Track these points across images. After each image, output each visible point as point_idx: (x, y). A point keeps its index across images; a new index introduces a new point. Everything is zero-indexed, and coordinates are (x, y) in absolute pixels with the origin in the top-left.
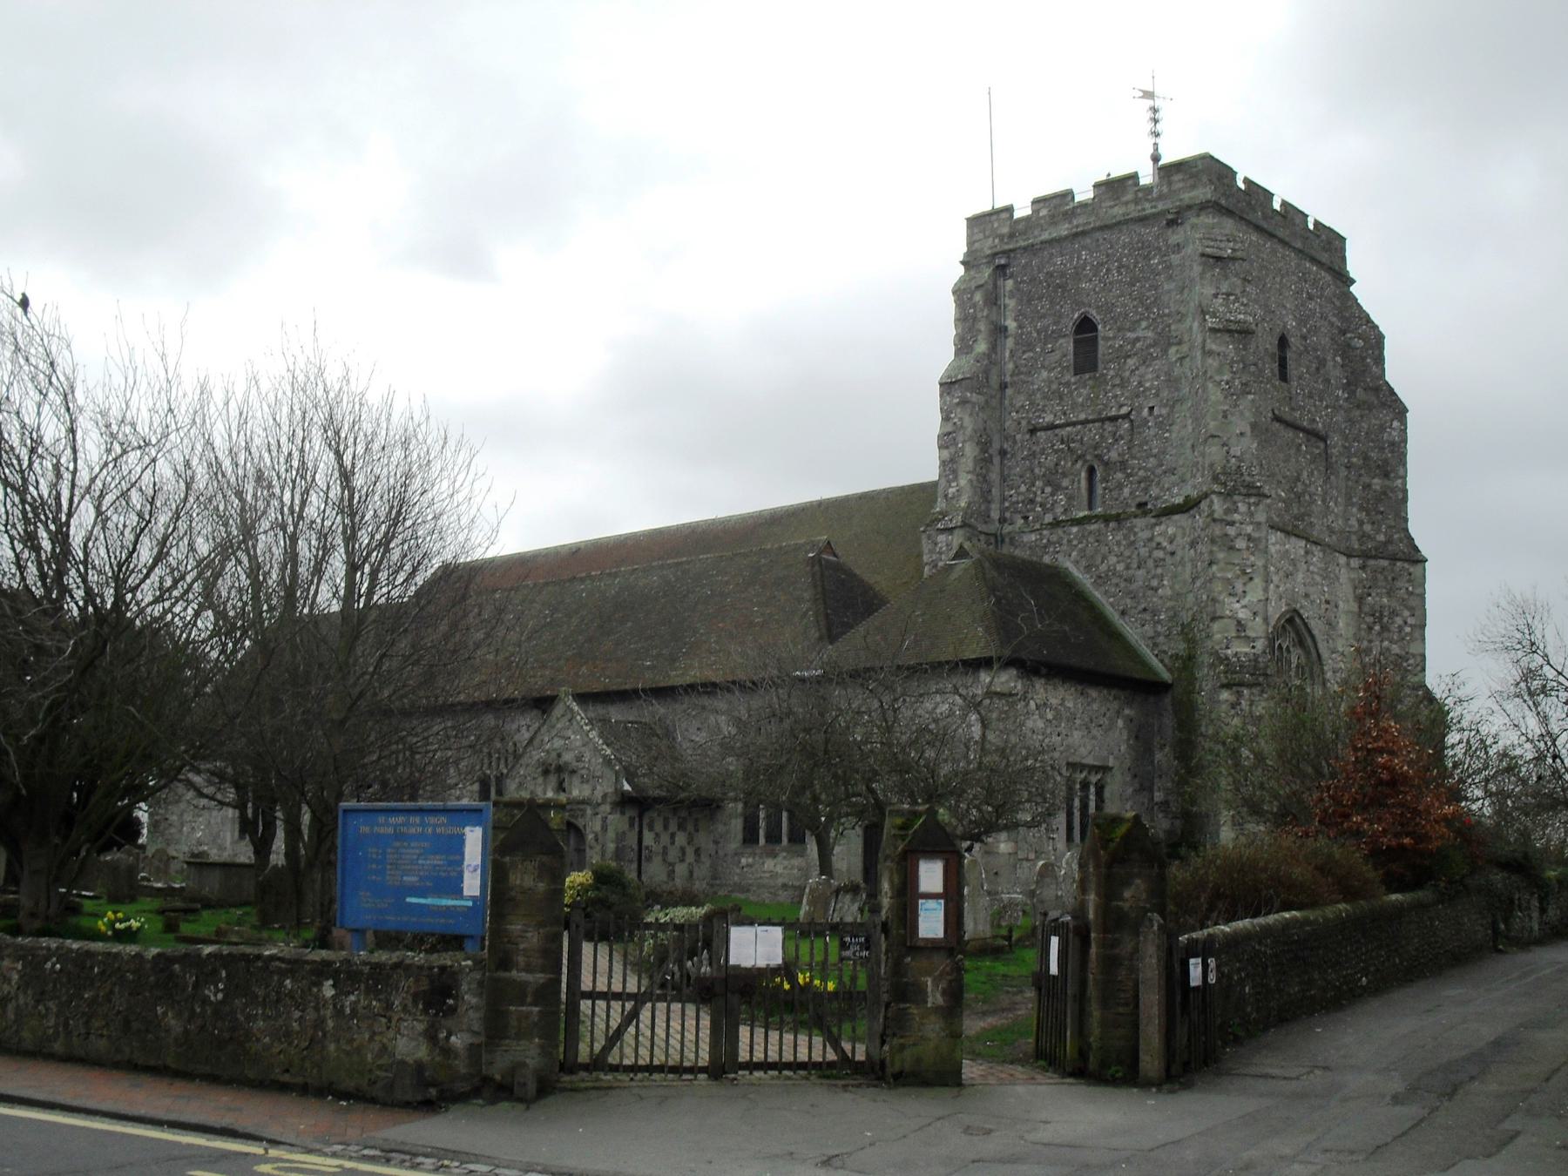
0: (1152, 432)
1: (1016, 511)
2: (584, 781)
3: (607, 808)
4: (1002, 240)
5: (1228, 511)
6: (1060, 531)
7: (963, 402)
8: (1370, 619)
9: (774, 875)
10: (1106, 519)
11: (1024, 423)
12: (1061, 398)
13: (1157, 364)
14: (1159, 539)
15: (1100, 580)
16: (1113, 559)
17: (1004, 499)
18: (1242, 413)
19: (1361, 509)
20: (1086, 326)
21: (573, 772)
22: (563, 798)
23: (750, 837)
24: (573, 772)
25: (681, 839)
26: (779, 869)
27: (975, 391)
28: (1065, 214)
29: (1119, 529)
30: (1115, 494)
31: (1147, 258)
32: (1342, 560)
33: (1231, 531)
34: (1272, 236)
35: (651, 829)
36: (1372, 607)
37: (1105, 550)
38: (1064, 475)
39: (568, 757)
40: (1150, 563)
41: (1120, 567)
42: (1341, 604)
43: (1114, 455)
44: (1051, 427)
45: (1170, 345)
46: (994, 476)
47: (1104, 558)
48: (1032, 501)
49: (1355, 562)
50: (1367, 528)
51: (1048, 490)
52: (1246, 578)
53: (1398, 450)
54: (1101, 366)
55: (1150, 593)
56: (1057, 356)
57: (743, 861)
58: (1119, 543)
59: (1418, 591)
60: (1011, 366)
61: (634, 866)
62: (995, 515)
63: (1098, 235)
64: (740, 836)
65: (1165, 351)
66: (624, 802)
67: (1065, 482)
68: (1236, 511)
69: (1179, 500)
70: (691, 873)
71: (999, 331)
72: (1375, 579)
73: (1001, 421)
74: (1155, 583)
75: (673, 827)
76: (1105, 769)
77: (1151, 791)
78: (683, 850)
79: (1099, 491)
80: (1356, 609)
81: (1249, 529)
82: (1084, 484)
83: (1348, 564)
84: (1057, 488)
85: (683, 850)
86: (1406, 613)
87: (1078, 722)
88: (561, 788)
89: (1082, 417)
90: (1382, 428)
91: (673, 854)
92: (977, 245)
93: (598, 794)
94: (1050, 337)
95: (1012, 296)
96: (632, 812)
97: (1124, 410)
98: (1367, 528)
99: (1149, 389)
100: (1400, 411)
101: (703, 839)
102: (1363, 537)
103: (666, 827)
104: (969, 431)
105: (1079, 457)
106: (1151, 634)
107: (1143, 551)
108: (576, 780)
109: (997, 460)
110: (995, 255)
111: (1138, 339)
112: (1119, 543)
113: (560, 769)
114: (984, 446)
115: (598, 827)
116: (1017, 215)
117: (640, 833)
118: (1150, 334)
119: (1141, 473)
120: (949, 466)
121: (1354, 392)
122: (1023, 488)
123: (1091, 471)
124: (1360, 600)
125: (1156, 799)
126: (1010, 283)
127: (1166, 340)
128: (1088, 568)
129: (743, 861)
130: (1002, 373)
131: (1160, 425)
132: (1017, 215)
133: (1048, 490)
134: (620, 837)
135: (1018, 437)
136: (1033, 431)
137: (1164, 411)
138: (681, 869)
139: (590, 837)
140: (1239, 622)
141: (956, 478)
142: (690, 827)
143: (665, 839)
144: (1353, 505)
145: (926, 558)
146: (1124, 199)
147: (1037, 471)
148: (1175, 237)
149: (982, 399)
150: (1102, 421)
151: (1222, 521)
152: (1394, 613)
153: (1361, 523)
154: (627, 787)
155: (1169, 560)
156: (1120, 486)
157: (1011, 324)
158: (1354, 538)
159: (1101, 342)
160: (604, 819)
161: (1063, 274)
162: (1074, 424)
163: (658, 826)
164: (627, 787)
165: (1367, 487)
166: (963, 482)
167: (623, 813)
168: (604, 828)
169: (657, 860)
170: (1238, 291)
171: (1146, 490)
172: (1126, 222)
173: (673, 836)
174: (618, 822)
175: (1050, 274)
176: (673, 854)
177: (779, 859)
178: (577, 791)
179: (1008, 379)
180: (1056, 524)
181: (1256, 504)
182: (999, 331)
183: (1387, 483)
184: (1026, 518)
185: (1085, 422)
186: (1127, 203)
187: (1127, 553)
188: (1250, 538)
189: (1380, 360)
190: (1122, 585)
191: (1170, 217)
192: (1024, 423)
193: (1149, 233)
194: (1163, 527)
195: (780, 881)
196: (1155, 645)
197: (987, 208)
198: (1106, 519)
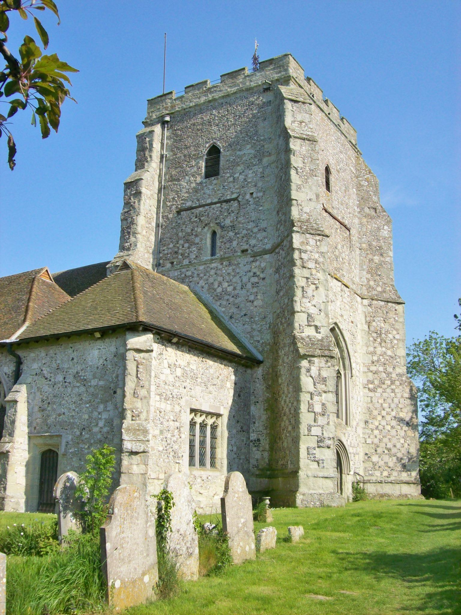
5: (302, 243)
6: (192, 269)
8: (375, 335)
11: (174, 207)
13: (255, 168)
16: (225, 285)
18: (310, 188)
19: (368, 272)
20: (214, 151)
29: (230, 264)
32: (359, 299)
34: (323, 111)
37: (220, 279)
38: (196, 236)
41: (230, 289)
42: (359, 326)
43: (228, 222)
48: (176, 253)
49: (366, 302)
50: (372, 283)
51: (186, 245)
54: (221, 172)
65: (260, 160)
67: (197, 240)
74: (252, 298)
76: (218, 415)
77: (248, 433)
79: (218, 244)
80: (367, 329)
81: (316, 256)
83: (362, 303)
84: (192, 244)
86: (395, 332)
87: (199, 380)
89: (209, 201)
90: (379, 229)
97: (234, 196)
98: (372, 283)
102: (370, 288)
105: (206, 225)
106: (249, 329)
107: (245, 279)
119: (245, 232)
121: (363, 209)
122: (171, 246)
123: (214, 233)
124: (369, 324)
125: (251, 438)
133: (186, 245)
144: (364, 270)
147: (180, 234)
152: (387, 332)
153: (369, 280)
155: (262, 283)
156: (231, 241)
158: (364, 288)
162: (203, 206)
165: (371, 260)
170: (306, 121)
183: (382, 259)
187: (234, 280)
188: (316, 262)
190: (232, 299)
194: (258, 263)
197: (162, 94)
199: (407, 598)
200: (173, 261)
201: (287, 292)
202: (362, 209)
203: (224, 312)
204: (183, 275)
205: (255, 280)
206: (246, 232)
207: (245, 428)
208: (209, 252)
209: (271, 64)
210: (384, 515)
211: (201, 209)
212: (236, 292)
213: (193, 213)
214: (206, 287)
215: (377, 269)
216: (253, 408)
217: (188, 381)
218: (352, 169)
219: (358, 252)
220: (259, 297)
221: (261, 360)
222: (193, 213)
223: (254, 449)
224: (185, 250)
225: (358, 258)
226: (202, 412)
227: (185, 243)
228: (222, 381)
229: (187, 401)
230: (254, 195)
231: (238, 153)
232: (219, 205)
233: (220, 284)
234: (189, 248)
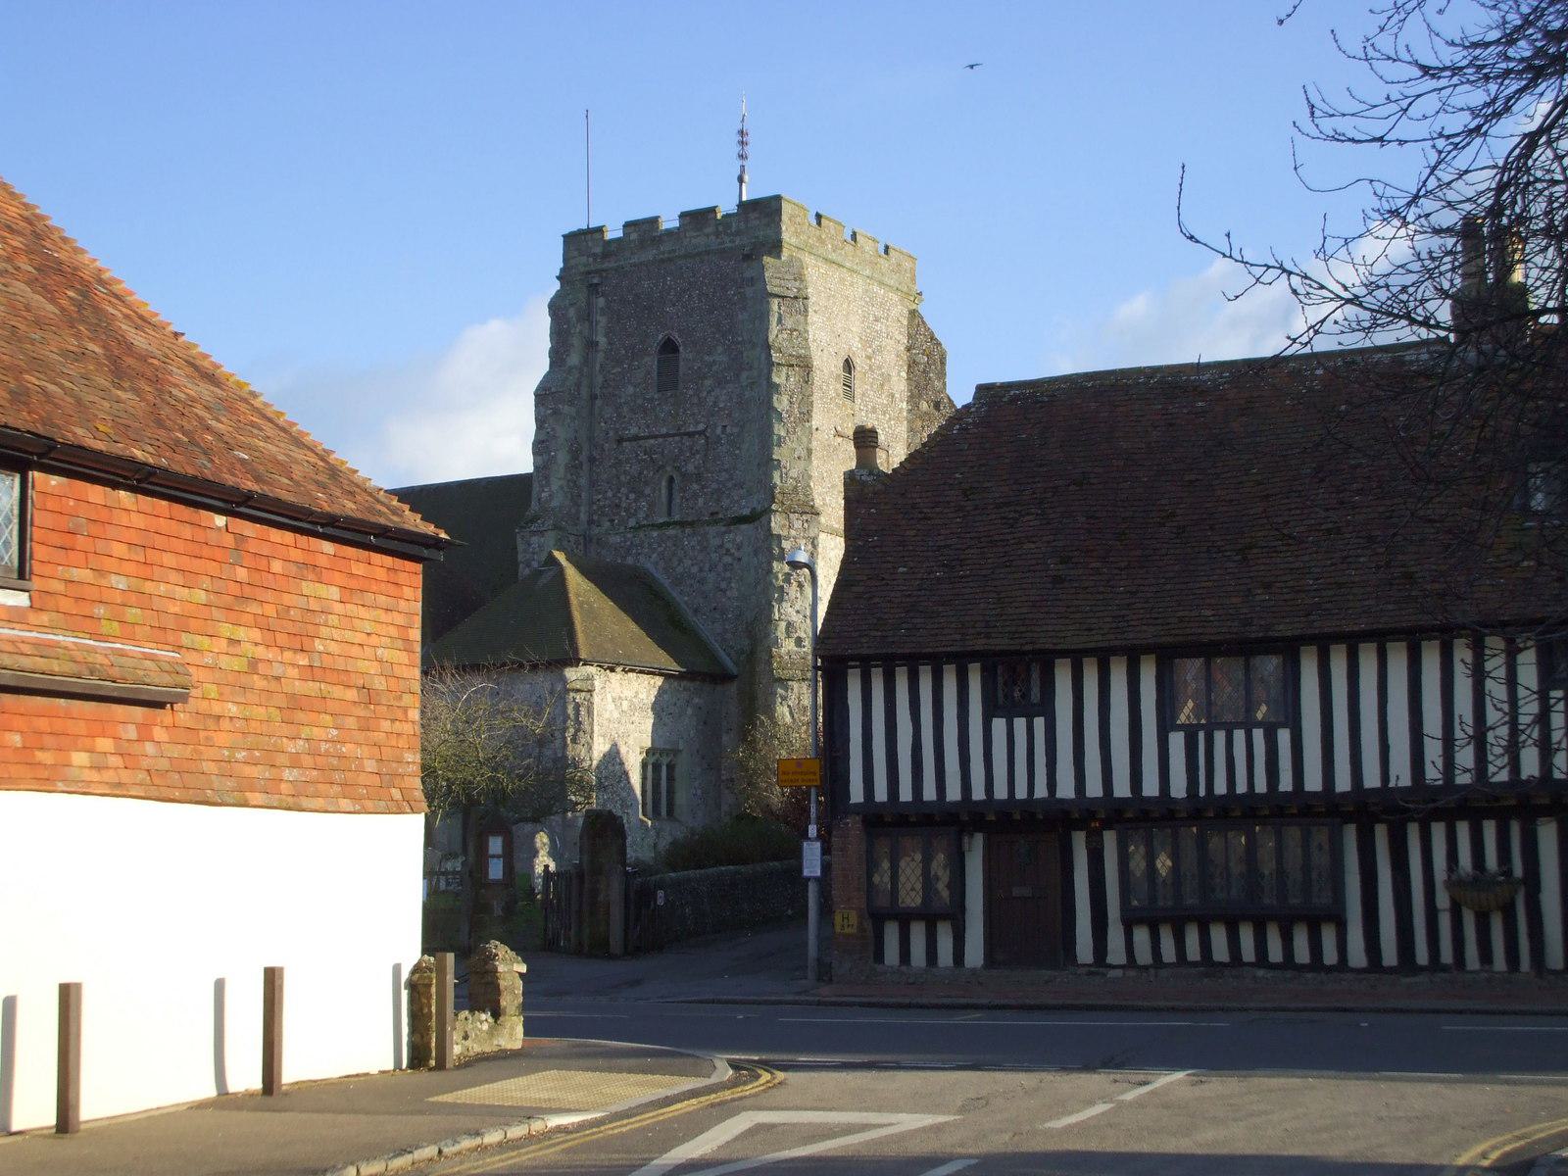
38: (646, 483)
48: (618, 506)
74: (723, 585)
84: (640, 494)
97: (701, 427)
123: (671, 480)
133: (632, 496)
147: (623, 478)
156: (695, 496)
200: (613, 518)
203: (686, 603)
204: (628, 543)
205: (728, 559)
206: (717, 486)
208: (665, 508)
209: (755, 210)
210: (99, 651)
211: (652, 441)
213: (640, 446)
214: (662, 564)
217: (637, 714)
220: (733, 585)
221: (736, 673)
222: (640, 446)
223: (727, 791)
224: (630, 504)
227: (631, 492)
229: (635, 739)
230: (728, 430)
231: (707, 358)
232: (677, 438)
233: (680, 561)
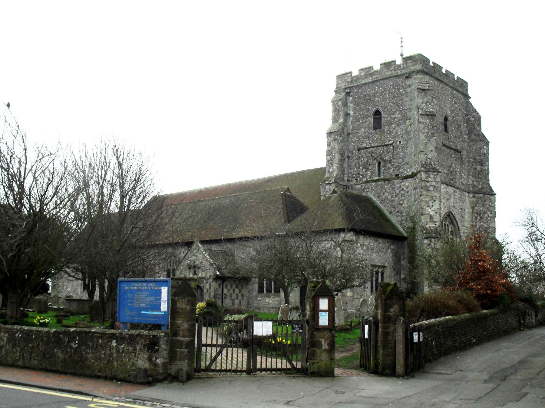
0: (401, 150)
1: (353, 178)
2: (203, 271)
3: (211, 280)
4: (348, 83)
5: (427, 177)
6: (368, 184)
7: (335, 140)
8: (476, 215)
9: (269, 304)
10: (385, 180)
11: (356, 147)
12: (369, 138)
13: (402, 126)
14: (403, 187)
15: (382, 201)
16: (387, 194)
17: (349, 173)
18: (432, 143)
19: (473, 176)
20: (377, 113)
21: (199, 268)
22: (196, 277)
23: (261, 291)
24: (199, 268)
25: (237, 291)
26: (271, 302)
27: (340, 136)
28: (370, 74)
29: (389, 183)
30: (388, 171)
31: (399, 89)
33: (428, 184)
35: (226, 287)
36: (477, 211)
38: (370, 165)
39: (197, 263)
40: (400, 195)
41: (389, 197)
43: (387, 158)
44: (366, 148)
45: (407, 120)
46: (346, 165)
47: (384, 194)
48: (359, 174)
49: (471, 195)
50: (475, 183)
52: (433, 201)
53: (486, 156)
55: (399, 206)
56: (367, 123)
57: (258, 299)
58: (389, 189)
59: (493, 205)
60: (351, 127)
61: (221, 300)
62: (346, 179)
63: (382, 81)
64: (257, 290)
65: (405, 122)
66: (217, 278)
67: (370, 167)
68: (430, 177)
69: (410, 173)
70: (240, 303)
71: (347, 115)
72: (478, 201)
73: (348, 146)
74: (401, 202)
75: (234, 287)
76: (384, 267)
77: (400, 274)
78: (237, 295)
80: (471, 211)
81: (434, 184)
82: (377, 168)
84: (367, 169)
85: (237, 295)
86: (489, 213)
87: (375, 250)
88: (195, 273)
89: (376, 145)
90: (480, 149)
91: (234, 297)
92: (340, 85)
93: (208, 275)
94: (365, 117)
95: (352, 103)
96: (219, 282)
97: (391, 142)
98: (475, 183)
99: (399, 135)
100: (487, 143)
101: (244, 291)
103: (231, 287)
104: (337, 150)
105: (375, 159)
106: (400, 220)
107: (397, 191)
108: (200, 271)
109: (346, 160)
110: (346, 88)
111: (395, 118)
112: (389, 189)
113: (194, 267)
114: (342, 155)
115: (208, 287)
116: (353, 75)
117: (223, 289)
118: (400, 116)
119: (397, 164)
120: (330, 162)
122: (356, 169)
123: (379, 163)
124: (473, 208)
125: (402, 277)
126: (351, 98)
127: (405, 118)
128: (378, 197)
129: (258, 299)
130: (348, 130)
131: (403, 148)
132: (353, 75)
133: (364, 170)
134: (216, 290)
135: (354, 152)
136: (359, 150)
137: (405, 143)
138: (237, 302)
139: (205, 290)
140: (431, 216)
141: (332, 166)
142: (240, 287)
143: (231, 291)
144: (470, 175)
145: (322, 194)
146: (391, 69)
147: (360, 163)
148: (409, 82)
149: (341, 138)
150: (383, 146)
151: (425, 181)
152: (484, 213)
153: (473, 181)
154: (218, 273)
155: (406, 194)
156: (389, 169)
157: (351, 113)
158: (471, 187)
159: (383, 119)
160: (210, 284)
161: (369, 95)
162: (373, 147)
163: (229, 287)
164: (218, 273)
165: (475, 169)
166: (335, 167)
167: (216, 282)
168: (210, 287)
169: (229, 298)
170: (430, 101)
171: (398, 170)
172: (392, 77)
173: (234, 290)
174: (215, 285)
175: (365, 95)
176: (234, 297)
177: (271, 298)
178: (201, 274)
179: (350, 132)
180: (367, 182)
181: (437, 175)
182: (347, 115)
183: (482, 167)
184: (357, 180)
185: (377, 147)
186: (391, 71)
187: (392, 192)
189: (480, 125)
190: (390, 203)
191: (407, 75)
192: (356, 147)
193: (399, 81)
194: (404, 183)
195: (271, 306)
196: (402, 224)
198: (385, 180)
199: (125, 156)
201: (419, 202)
202: (470, 137)
205: (403, 192)
207: (398, 272)
212: (393, 198)
215: (479, 173)
216: (403, 262)
218: (464, 111)
219: (467, 164)
225: (466, 168)
226: (376, 266)
228: (386, 250)
234: (366, 172)
